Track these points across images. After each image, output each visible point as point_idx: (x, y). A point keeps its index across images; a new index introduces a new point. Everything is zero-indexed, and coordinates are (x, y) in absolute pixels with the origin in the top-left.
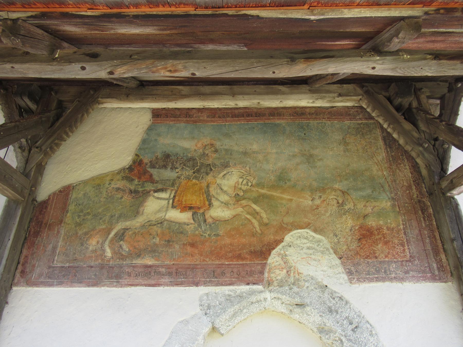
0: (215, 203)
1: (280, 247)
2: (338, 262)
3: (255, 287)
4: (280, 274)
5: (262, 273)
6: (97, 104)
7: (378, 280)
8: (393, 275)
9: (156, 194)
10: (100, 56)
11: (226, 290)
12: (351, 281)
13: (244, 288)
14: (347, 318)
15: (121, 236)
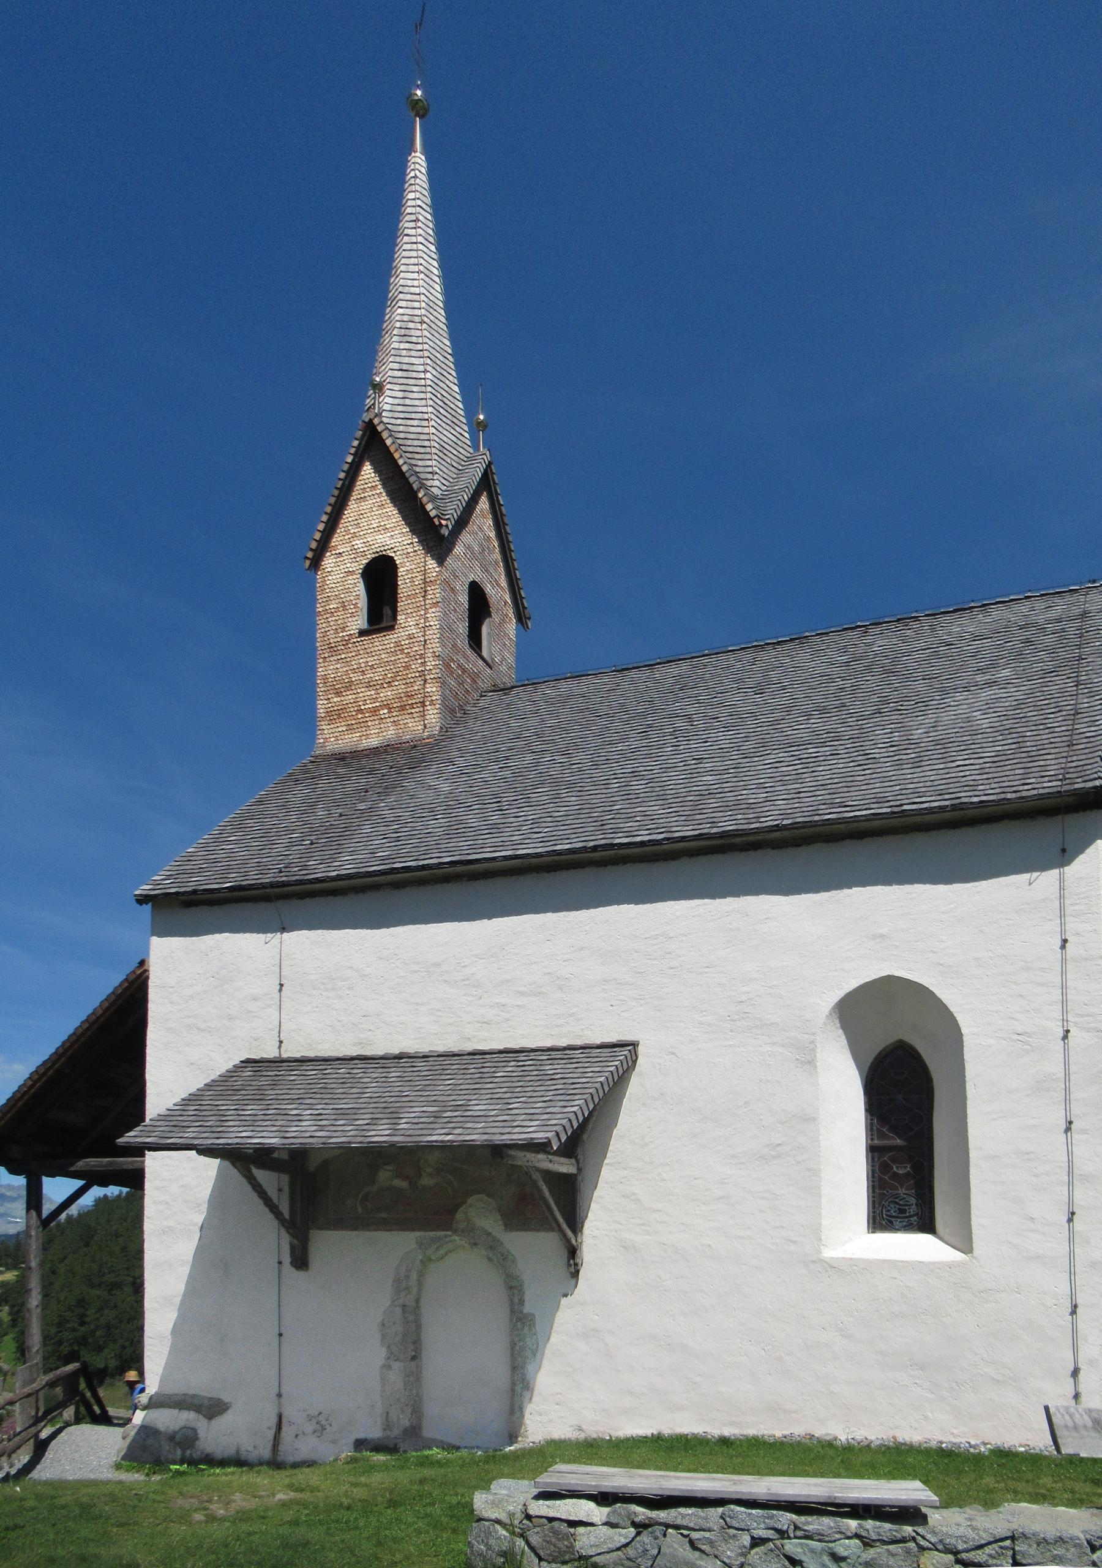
0: (423, 1174)
1: (464, 1206)
2: (500, 1217)
3: (448, 1233)
4: (463, 1225)
5: (451, 1224)
6: (197, 1442)
7: (522, 1230)
8: (533, 1227)
9: (385, 1167)
10: (228, 1408)
11: (431, 1234)
12: (505, 1229)
13: (440, 1233)
14: (500, 1252)
15: (365, 1198)
